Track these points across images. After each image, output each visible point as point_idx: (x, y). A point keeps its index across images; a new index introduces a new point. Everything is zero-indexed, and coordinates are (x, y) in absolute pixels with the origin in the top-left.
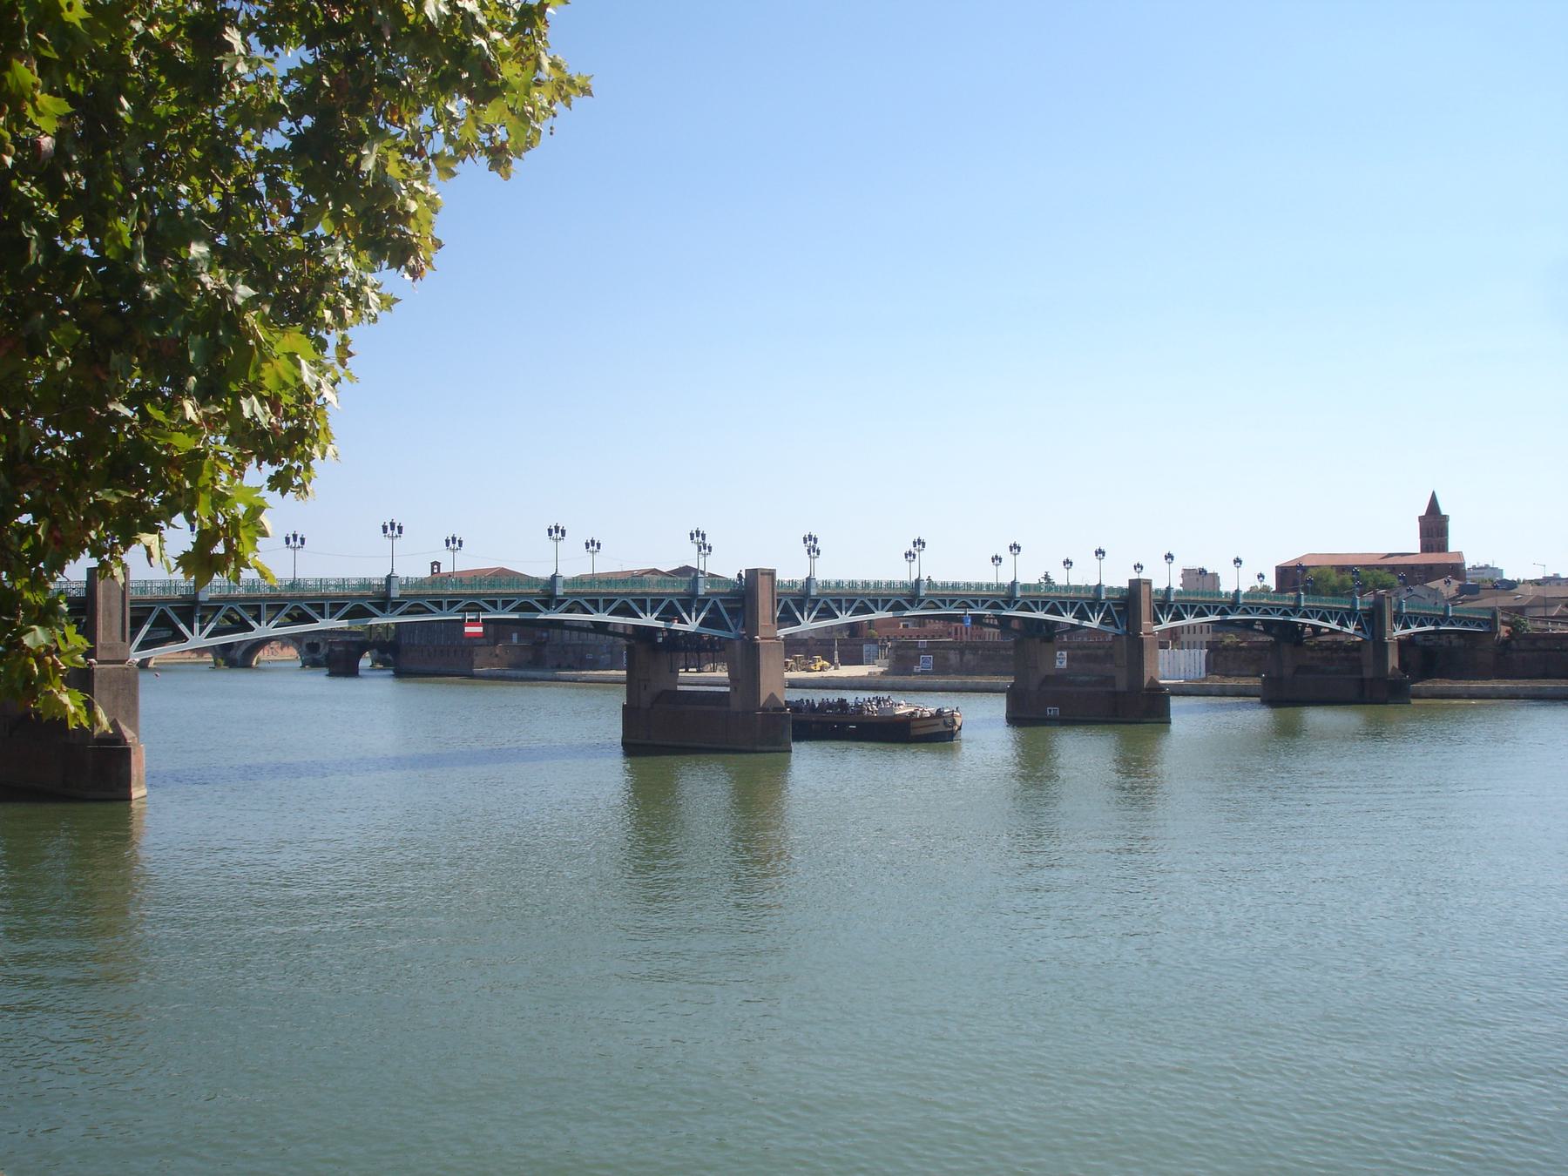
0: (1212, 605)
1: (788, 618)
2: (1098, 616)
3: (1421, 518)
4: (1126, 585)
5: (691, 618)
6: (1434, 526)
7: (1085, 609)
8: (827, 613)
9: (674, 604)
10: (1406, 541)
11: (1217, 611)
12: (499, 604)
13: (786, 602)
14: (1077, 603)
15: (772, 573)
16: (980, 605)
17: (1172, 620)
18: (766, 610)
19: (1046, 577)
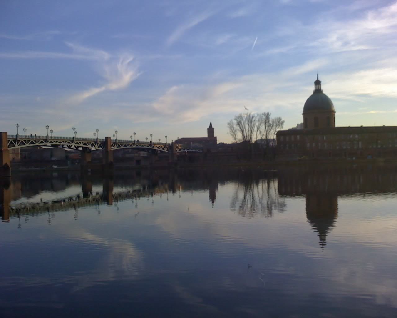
0: (89, 142)
1: (12, 144)
2: (97, 145)
3: (208, 129)
4: (104, 138)
5: (16, 144)
6: (211, 130)
8: (119, 146)
9: (23, 142)
10: (205, 135)
11: (30, 142)
13: (11, 141)
14: (20, 141)
16: (37, 142)
17: (117, 147)
18: (109, 144)
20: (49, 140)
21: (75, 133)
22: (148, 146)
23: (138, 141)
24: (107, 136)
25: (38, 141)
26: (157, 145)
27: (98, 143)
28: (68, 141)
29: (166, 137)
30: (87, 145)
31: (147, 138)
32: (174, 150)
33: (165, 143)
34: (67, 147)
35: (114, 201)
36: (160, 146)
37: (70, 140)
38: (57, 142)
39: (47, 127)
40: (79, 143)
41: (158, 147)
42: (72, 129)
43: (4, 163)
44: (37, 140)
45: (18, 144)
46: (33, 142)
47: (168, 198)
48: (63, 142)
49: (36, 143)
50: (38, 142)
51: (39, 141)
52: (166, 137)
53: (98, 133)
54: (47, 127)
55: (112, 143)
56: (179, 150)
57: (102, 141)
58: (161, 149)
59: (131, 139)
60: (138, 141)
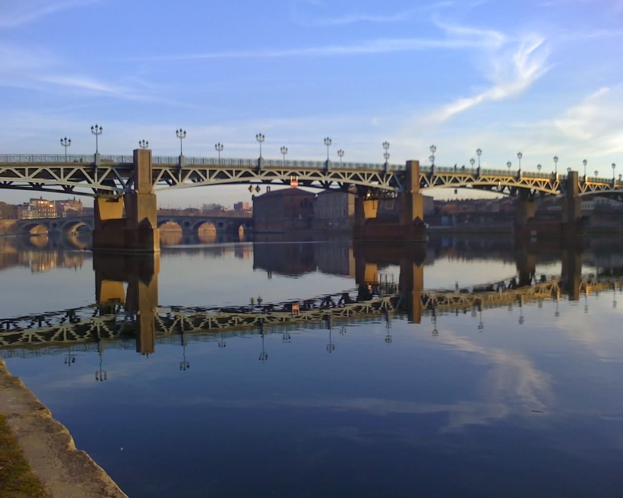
4: (404, 163)
5: (383, 181)
7: (159, 174)
12: (282, 173)
13: (166, 171)
14: (189, 170)
15: (417, 162)
19: (455, 166)
20: (265, 167)
21: (387, 155)
22: (511, 181)
23: (463, 167)
24: (409, 159)
25: (237, 172)
26: (596, 182)
27: (389, 175)
28: (312, 172)
29: (614, 165)
30: (228, 177)
31: (509, 164)
32: (575, 189)
33: (611, 178)
34: (322, 186)
35: (29, 470)
36: (540, 182)
37: (319, 169)
38: (307, 173)
39: (328, 141)
40: (341, 175)
41: (598, 187)
42: (323, 141)
43: (414, 217)
44: (234, 170)
45: (433, 181)
46: (358, 177)
47: (586, 306)
48: (300, 174)
49: (232, 175)
50: (348, 176)
51: (240, 171)
52: (614, 165)
53: (481, 157)
54: (259, 138)
55: (423, 175)
56: (586, 191)
57: (397, 169)
58: (542, 188)
59: (339, 158)
60: (463, 167)
